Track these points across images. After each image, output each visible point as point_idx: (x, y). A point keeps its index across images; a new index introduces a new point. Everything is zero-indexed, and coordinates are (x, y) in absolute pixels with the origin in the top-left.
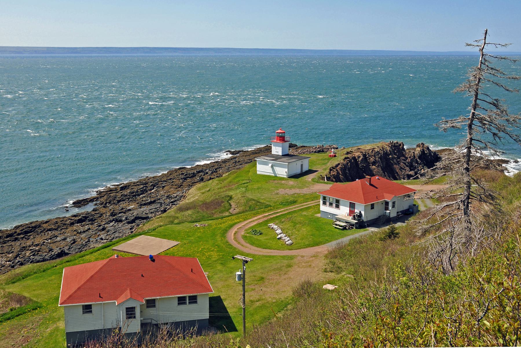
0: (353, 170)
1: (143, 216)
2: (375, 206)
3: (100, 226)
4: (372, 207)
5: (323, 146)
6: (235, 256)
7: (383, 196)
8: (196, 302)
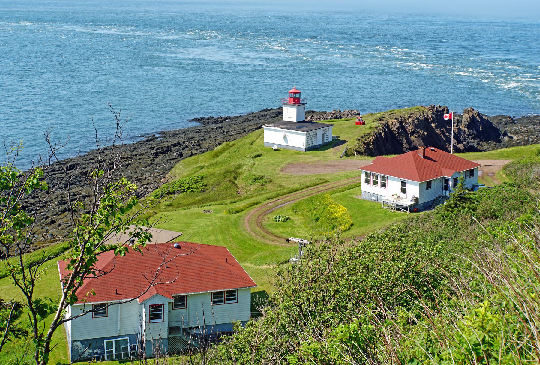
0: (386, 143)
3: (47, 218)
4: (429, 185)
5: (340, 111)
6: (289, 239)
7: (441, 171)
8: (184, 305)
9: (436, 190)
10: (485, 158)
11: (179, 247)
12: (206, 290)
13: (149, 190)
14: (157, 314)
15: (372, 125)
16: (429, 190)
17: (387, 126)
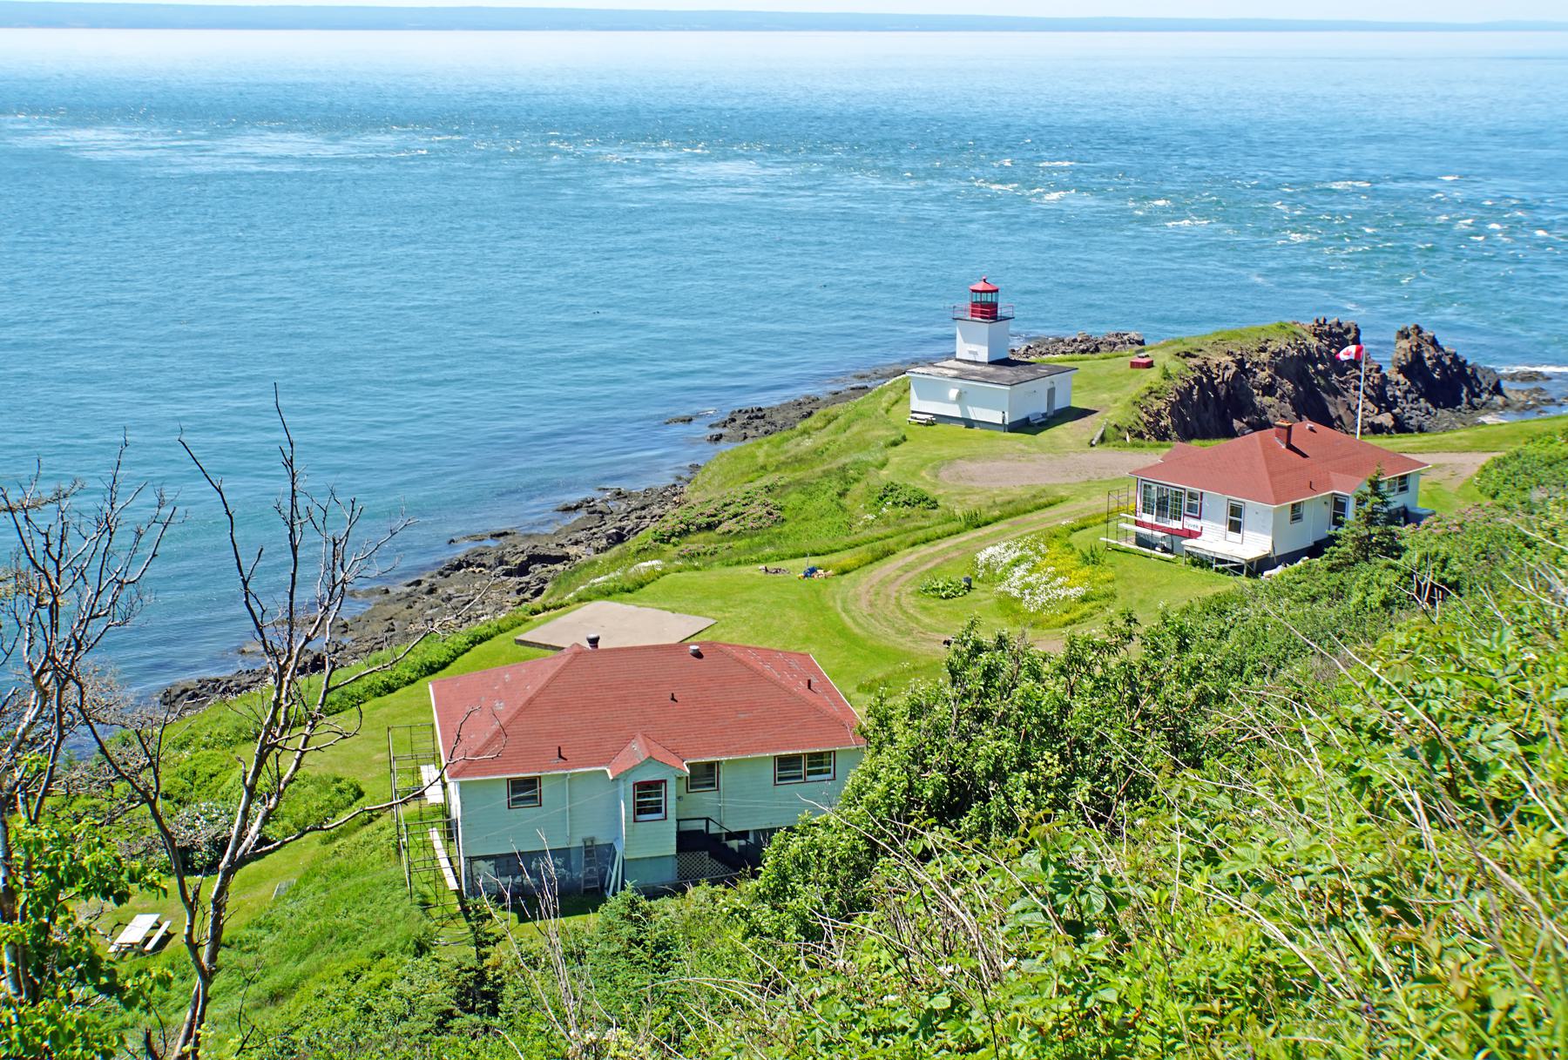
0: (1210, 408)
1: (553, 554)
2: (1306, 512)
8: (535, 800)
9: (1315, 525)
10: (1433, 449)
11: (698, 655)
13: (647, 521)
15: (1169, 367)
16: (1298, 524)
17: (1204, 369)
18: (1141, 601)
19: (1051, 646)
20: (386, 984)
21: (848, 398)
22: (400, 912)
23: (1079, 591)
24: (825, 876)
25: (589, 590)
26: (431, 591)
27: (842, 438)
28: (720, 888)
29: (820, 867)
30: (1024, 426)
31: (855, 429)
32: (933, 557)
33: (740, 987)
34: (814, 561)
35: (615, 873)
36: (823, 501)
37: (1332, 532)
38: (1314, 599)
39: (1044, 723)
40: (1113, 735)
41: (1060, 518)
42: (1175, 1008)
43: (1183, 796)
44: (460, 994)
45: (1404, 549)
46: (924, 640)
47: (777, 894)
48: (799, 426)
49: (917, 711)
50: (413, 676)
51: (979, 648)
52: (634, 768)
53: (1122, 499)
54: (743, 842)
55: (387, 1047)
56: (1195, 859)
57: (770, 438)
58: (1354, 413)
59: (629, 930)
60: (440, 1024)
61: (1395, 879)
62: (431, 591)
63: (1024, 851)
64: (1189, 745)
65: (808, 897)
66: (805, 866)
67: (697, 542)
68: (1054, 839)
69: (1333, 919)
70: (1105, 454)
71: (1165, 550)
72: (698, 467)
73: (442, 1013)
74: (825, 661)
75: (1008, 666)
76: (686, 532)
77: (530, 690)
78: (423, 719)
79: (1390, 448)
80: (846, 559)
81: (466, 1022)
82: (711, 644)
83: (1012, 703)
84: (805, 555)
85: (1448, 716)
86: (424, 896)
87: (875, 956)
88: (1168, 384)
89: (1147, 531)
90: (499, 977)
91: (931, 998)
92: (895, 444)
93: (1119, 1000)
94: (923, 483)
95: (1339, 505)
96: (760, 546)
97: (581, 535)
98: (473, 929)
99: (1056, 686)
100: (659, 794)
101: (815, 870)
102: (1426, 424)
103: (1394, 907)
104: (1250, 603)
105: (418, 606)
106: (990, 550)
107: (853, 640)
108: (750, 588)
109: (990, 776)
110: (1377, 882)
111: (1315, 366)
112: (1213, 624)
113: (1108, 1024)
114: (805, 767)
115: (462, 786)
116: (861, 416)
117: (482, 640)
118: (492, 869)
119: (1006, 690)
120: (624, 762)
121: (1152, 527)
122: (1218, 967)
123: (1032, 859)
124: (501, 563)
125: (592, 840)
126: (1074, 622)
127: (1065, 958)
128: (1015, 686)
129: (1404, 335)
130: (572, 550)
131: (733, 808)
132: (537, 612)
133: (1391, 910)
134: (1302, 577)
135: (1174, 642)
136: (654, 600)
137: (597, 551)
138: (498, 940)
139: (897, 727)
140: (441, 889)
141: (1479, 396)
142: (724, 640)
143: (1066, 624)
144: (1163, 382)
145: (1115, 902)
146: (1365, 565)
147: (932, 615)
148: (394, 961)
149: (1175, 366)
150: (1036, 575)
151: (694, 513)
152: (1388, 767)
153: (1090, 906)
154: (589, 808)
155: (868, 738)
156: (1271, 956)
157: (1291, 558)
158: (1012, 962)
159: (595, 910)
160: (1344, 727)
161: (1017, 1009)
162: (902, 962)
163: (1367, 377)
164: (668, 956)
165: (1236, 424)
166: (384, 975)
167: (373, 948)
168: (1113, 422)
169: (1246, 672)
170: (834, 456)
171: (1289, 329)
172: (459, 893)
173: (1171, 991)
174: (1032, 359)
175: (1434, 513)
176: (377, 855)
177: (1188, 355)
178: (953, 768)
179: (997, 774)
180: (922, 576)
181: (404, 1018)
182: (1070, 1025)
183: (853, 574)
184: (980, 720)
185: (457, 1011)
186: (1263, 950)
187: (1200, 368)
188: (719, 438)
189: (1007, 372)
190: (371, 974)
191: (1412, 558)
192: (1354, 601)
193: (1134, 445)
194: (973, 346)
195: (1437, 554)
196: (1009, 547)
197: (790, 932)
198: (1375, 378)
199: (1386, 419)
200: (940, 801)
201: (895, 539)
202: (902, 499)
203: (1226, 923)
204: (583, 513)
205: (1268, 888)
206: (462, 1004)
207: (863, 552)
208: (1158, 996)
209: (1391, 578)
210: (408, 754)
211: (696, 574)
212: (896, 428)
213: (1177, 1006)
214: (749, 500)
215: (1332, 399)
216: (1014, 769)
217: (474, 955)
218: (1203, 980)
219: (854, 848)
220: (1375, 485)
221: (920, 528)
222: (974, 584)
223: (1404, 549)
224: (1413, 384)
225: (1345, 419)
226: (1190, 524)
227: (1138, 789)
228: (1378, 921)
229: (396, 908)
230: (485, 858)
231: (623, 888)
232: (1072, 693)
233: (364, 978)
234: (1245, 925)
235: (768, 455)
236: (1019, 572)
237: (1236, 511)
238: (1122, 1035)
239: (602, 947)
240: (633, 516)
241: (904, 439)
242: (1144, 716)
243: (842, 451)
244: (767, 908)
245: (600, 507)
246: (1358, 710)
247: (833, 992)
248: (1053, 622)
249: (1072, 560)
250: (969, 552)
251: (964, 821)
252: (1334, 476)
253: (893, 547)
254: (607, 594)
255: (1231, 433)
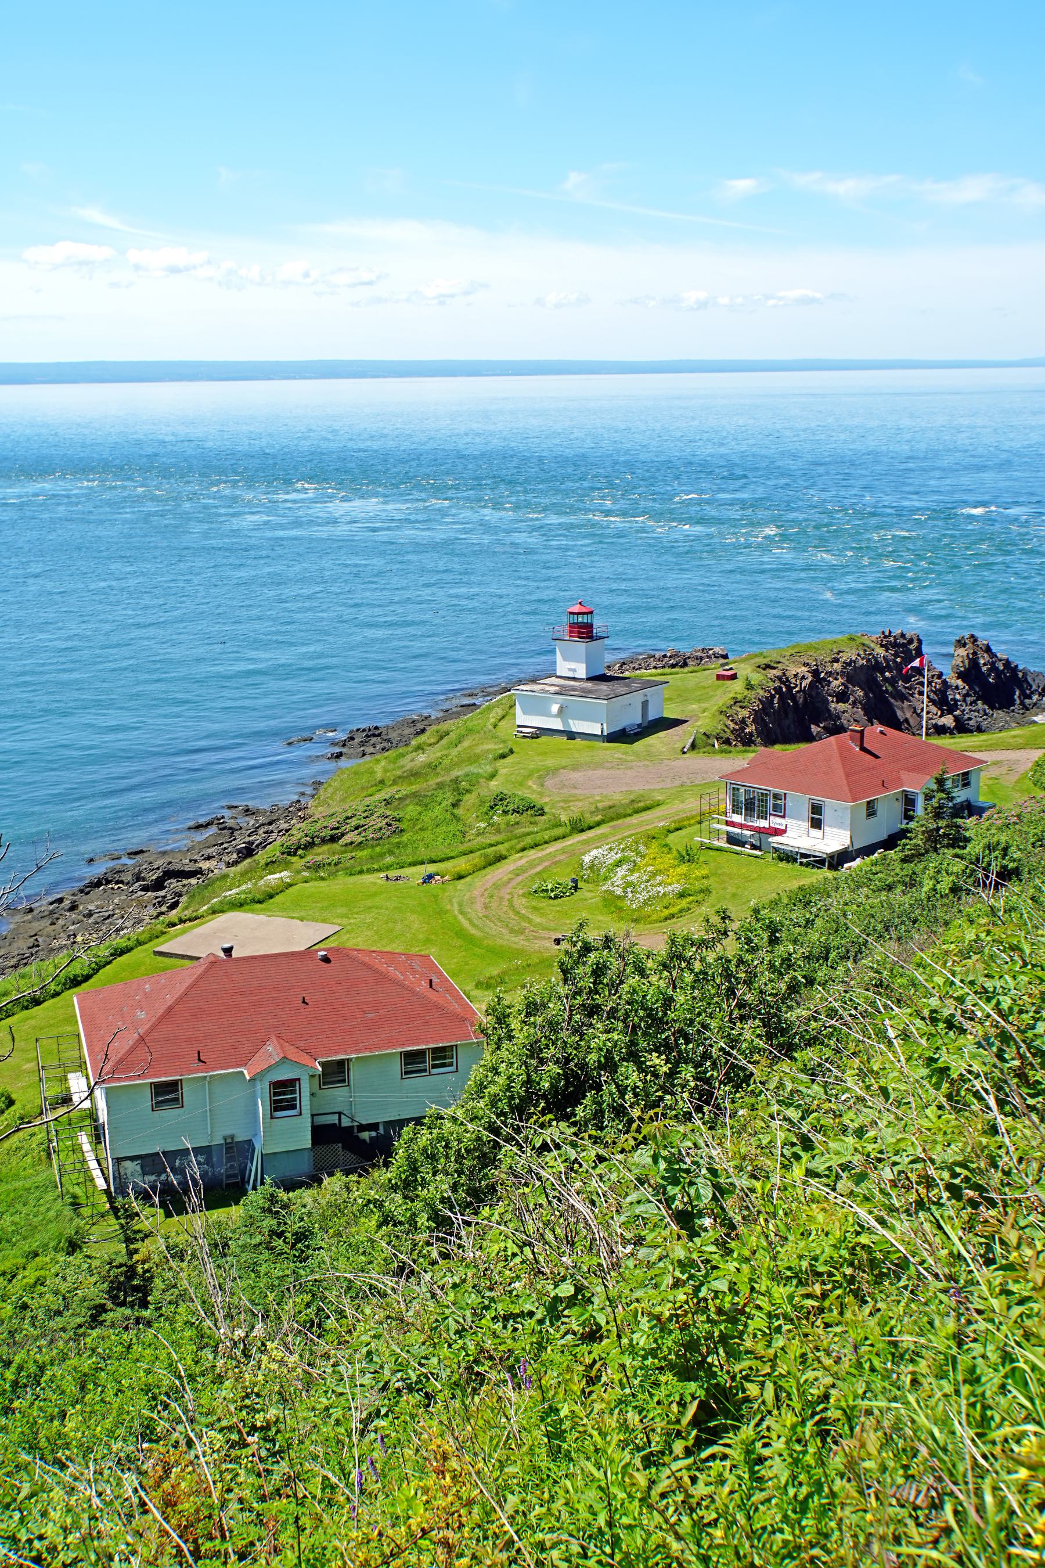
0: (789, 715)
1: (187, 869)
2: (881, 809)
4: (871, 810)
7: (899, 779)
10: (991, 748)
11: (326, 960)
12: (389, 1047)
14: (287, 1100)
17: (783, 679)
18: (734, 895)
19: (653, 943)
20: (40, 1282)
21: (458, 715)
22: (52, 1213)
23: (676, 888)
24: (452, 1166)
25: (221, 902)
26: (73, 908)
27: (454, 752)
28: (353, 1177)
29: (447, 1157)
30: (621, 736)
31: (466, 744)
32: (541, 860)
33: (375, 1276)
34: (431, 868)
35: (255, 1166)
36: (438, 812)
37: (903, 826)
38: (890, 888)
39: (649, 1016)
40: (714, 1024)
41: (655, 820)
42: (780, 1292)
43: (781, 1085)
44: (111, 1289)
45: (968, 840)
46: (536, 938)
47: (408, 1185)
48: (414, 743)
49: (532, 1008)
50: (58, 989)
51: (587, 949)
52: (270, 1069)
53: (713, 802)
54: (374, 1134)
55: (43, 1342)
56: (793, 1144)
57: (386, 754)
58: (919, 716)
59: (269, 1222)
60: (94, 1318)
61: (974, 1166)
62: (73, 908)
63: (637, 1145)
64: (783, 1032)
65: (439, 1187)
66: (432, 1158)
67: (321, 853)
68: (664, 1137)
69: (920, 1204)
70: (697, 761)
71: (754, 847)
72: (320, 783)
73: (95, 1307)
74: (445, 961)
75: (615, 964)
76: (311, 845)
77: (170, 999)
78: (69, 1029)
79: (953, 747)
80: (462, 864)
81: (118, 1315)
82: (338, 950)
83: (620, 997)
84: (422, 863)
85: (1016, 1009)
86: (75, 1197)
87: (502, 1245)
88: (751, 694)
89: (738, 831)
90: (148, 1271)
91: (556, 1286)
92: (503, 756)
93: (730, 1289)
94: (531, 792)
95: (909, 801)
96: (382, 855)
97: (212, 851)
98: (122, 1227)
99: (659, 981)
100: (293, 1092)
101: (442, 1160)
102: (984, 724)
103: (971, 1190)
104: (832, 893)
105: (61, 922)
106: (594, 853)
107: (470, 940)
108: (374, 895)
109: (601, 1067)
110: (958, 1170)
111: (882, 674)
112: (799, 914)
113: (720, 1311)
114: (429, 1061)
115: (108, 1093)
116: (470, 731)
117: (122, 952)
118: (138, 1168)
119: (614, 988)
120: (259, 1063)
121: (742, 826)
122: (818, 1252)
123: (643, 1156)
124: (138, 880)
125: (232, 1137)
126: (673, 916)
127: (679, 1252)
128: (622, 982)
129: (961, 643)
130: (205, 865)
131: (366, 1102)
132: (174, 925)
133: (971, 1193)
134: (878, 868)
135: (766, 935)
136: (284, 911)
137: (228, 865)
138: (146, 1236)
139: (515, 1024)
140: (90, 1190)
141: (1030, 698)
142: (350, 944)
143: (666, 919)
144: (746, 692)
145: (720, 1191)
146: (934, 855)
147: (542, 915)
148: (47, 1259)
149: (756, 678)
150: (636, 875)
151: (318, 825)
152: (964, 1057)
153: (698, 1196)
154: (227, 1106)
155: (487, 1035)
156: (864, 1239)
157: (867, 851)
158: (629, 1249)
159: (237, 1203)
160: (923, 1019)
161: (638, 1301)
162: (527, 1250)
163: (930, 683)
164: (308, 1247)
165: (814, 729)
166: (38, 1273)
167: (26, 1248)
168: (702, 731)
169: (831, 957)
170: (448, 770)
171: (859, 641)
172: (107, 1192)
173: (776, 1277)
174: (627, 674)
175: (994, 806)
176: (28, 1160)
177: (768, 667)
178: (568, 1060)
179: (609, 1065)
180: (532, 879)
181: (59, 1313)
182: (686, 1313)
183: (468, 879)
184: (590, 1015)
185: (110, 1305)
186: (858, 1233)
187: (779, 678)
188: (339, 755)
189: (604, 687)
190: (26, 1273)
191: (974, 848)
192: (925, 889)
193: (722, 752)
194: (571, 664)
195: (998, 843)
196: (611, 849)
197: (422, 1220)
198: (937, 683)
199: (948, 721)
200: (556, 1091)
201: (506, 845)
202: (511, 807)
203: (824, 1210)
204: (213, 830)
205: (861, 1178)
206: (114, 1298)
207: (476, 858)
208: (763, 1285)
209: (958, 867)
210: (56, 1063)
211: (322, 884)
212: (504, 742)
213: (782, 1289)
214: (369, 812)
215: (899, 703)
216: (623, 1059)
217: (124, 1251)
218: (805, 1264)
219: (479, 1139)
220: (940, 782)
221: (528, 834)
222: (580, 885)
223: (968, 840)
224: (971, 688)
225: (911, 721)
226: (776, 822)
227: (739, 1079)
228: (961, 1204)
229: (49, 1209)
230: (132, 1158)
231: (263, 1183)
232: (675, 987)
233: (20, 1277)
234: (841, 1212)
235: (386, 771)
236: (621, 872)
237: (816, 809)
238: (734, 1321)
239: (245, 1239)
240: (261, 831)
241: (511, 752)
242: (741, 1005)
243: (454, 765)
244: (398, 1198)
245: (230, 823)
246: (934, 1002)
247: (464, 1281)
248: (654, 917)
249: (669, 859)
250: (573, 854)
251: (579, 1110)
252: (905, 776)
253: (504, 853)
254: (239, 905)
255: (810, 738)
